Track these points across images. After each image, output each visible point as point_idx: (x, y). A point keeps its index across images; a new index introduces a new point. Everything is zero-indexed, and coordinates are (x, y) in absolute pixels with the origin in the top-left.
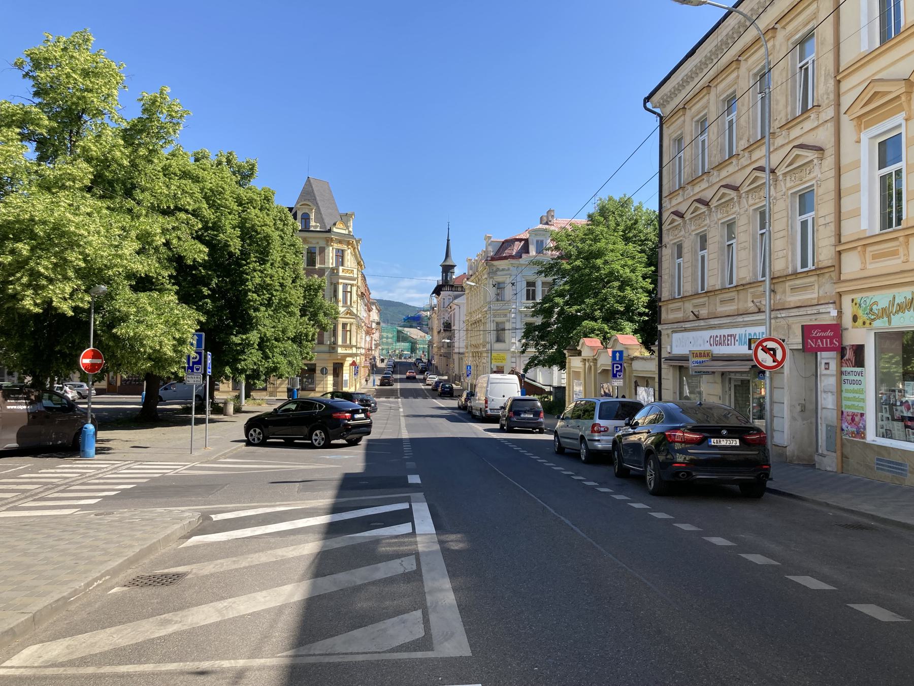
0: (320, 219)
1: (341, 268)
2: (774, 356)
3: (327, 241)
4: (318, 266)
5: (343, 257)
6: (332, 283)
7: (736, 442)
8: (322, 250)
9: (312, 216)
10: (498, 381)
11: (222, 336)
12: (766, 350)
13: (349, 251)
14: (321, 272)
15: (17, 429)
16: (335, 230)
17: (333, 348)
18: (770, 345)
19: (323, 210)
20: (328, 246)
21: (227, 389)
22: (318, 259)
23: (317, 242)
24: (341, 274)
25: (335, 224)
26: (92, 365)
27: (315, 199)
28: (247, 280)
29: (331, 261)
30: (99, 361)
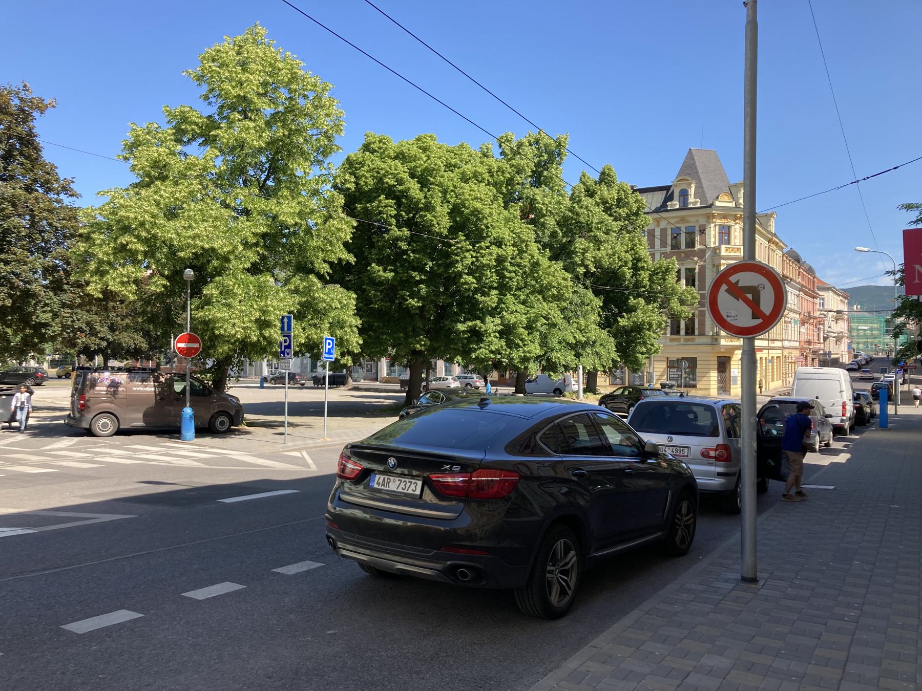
0: (700, 193)
1: (723, 247)
2: (754, 305)
3: (708, 217)
4: (698, 247)
5: (729, 234)
6: (714, 266)
7: (414, 487)
8: (702, 231)
9: (692, 191)
10: (809, 376)
11: (447, 322)
12: (737, 292)
13: (737, 227)
14: (701, 254)
15: (143, 410)
16: (717, 204)
17: (716, 340)
18: (746, 279)
19: (705, 184)
20: (709, 223)
21: (604, 384)
22: (698, 238)
23: (694, 221)
24: (723, 253)
25: (717, 198)
26: (188, 349)
27: (697, 172)
28: (457, 261)
29: (713, 240)
30: (196, 345)
